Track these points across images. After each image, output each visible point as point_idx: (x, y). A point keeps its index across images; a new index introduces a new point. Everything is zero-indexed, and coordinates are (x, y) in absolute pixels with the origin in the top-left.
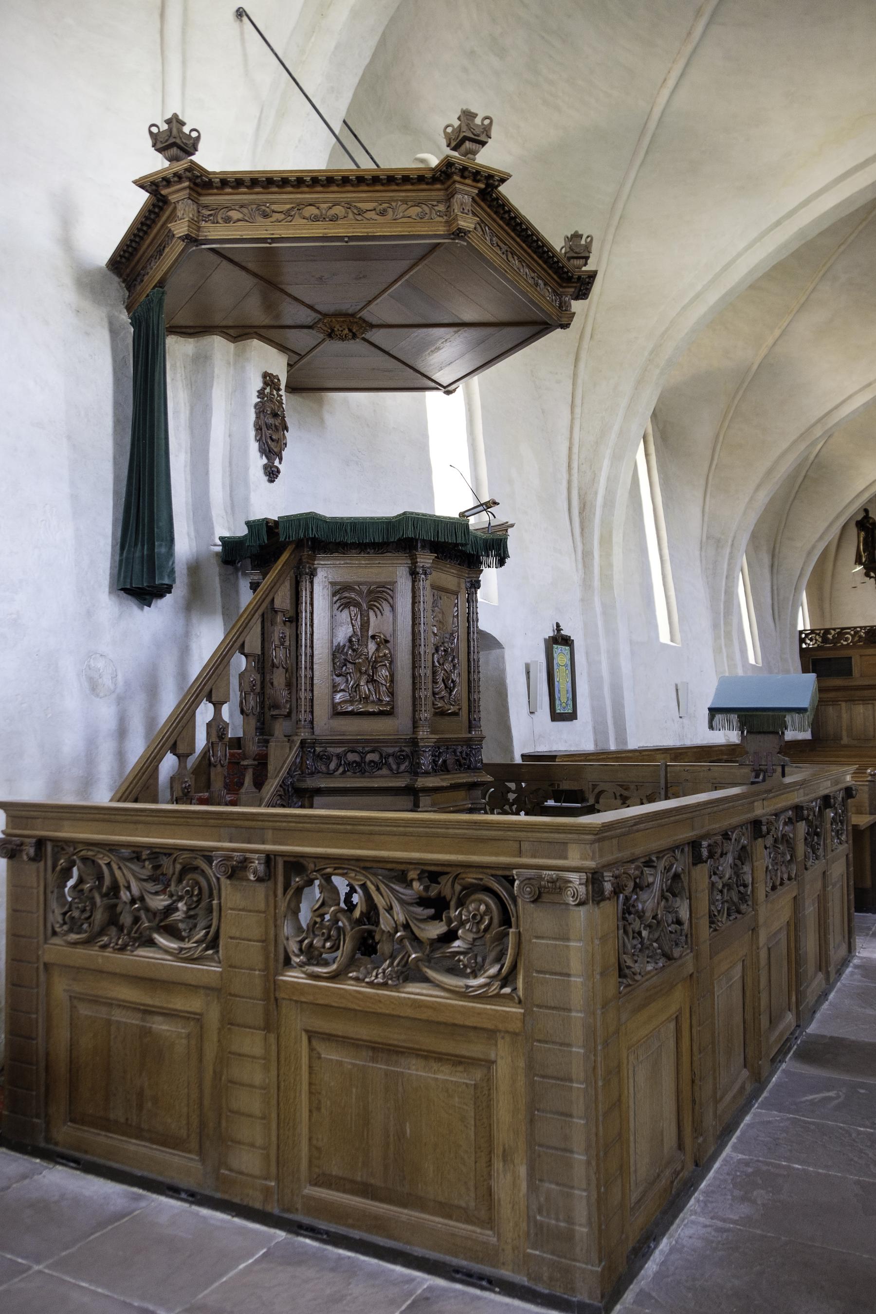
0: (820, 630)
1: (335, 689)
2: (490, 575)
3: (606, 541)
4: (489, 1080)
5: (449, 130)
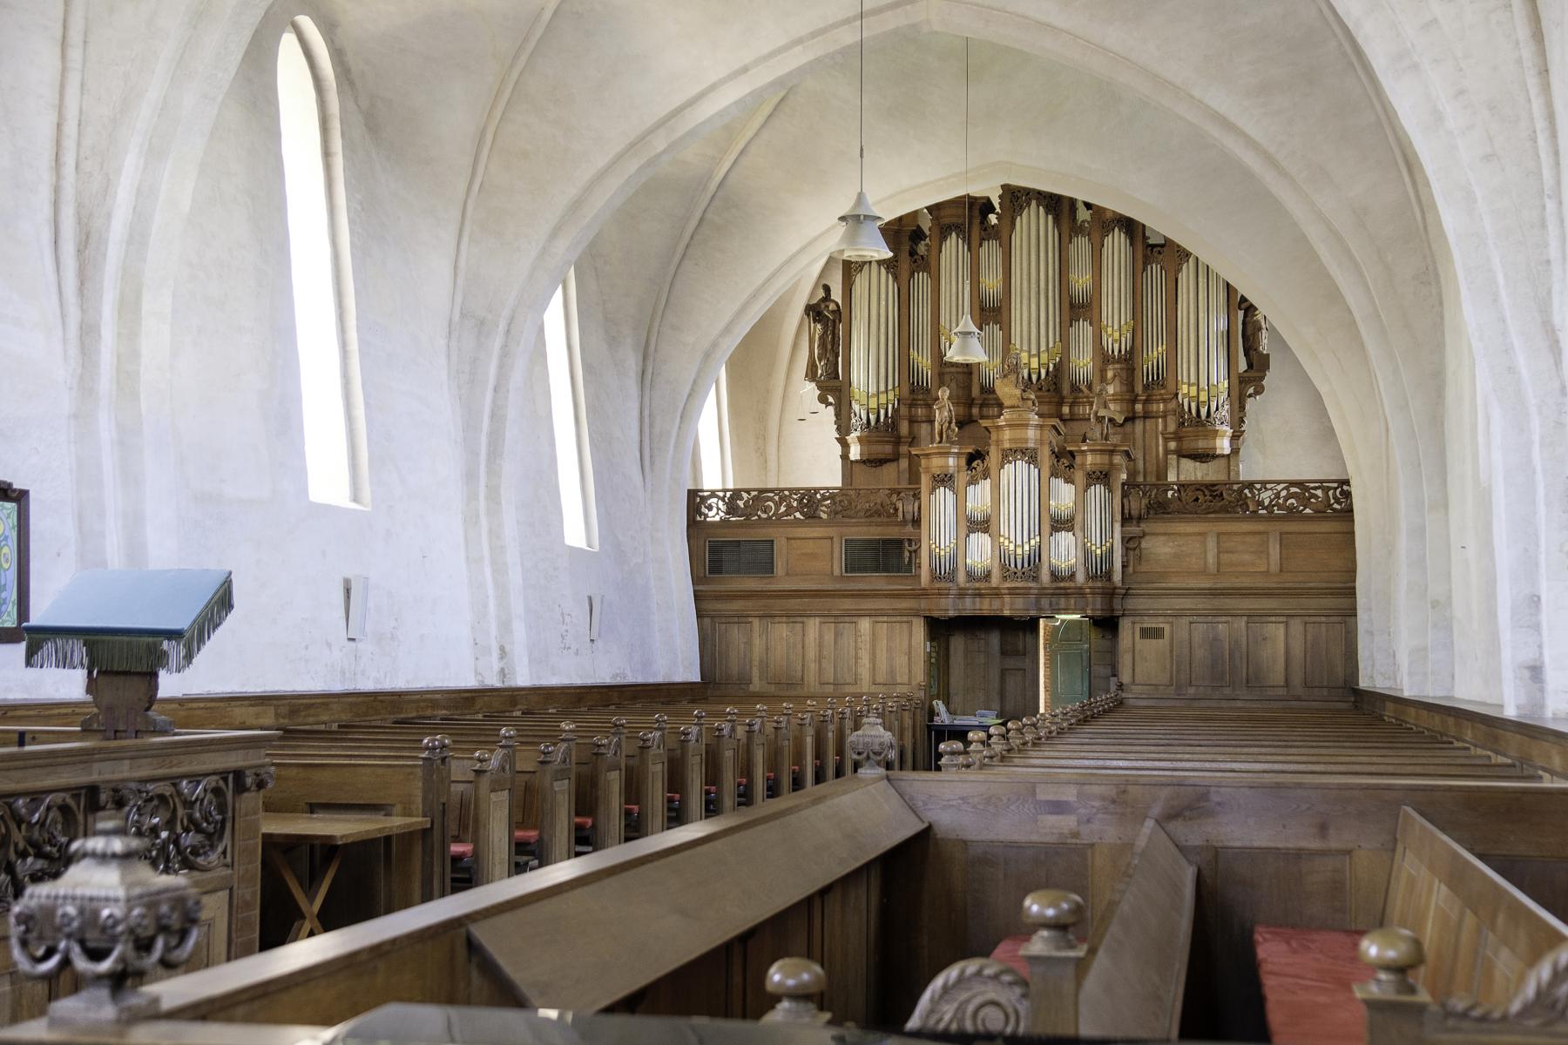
3: (130, 308)
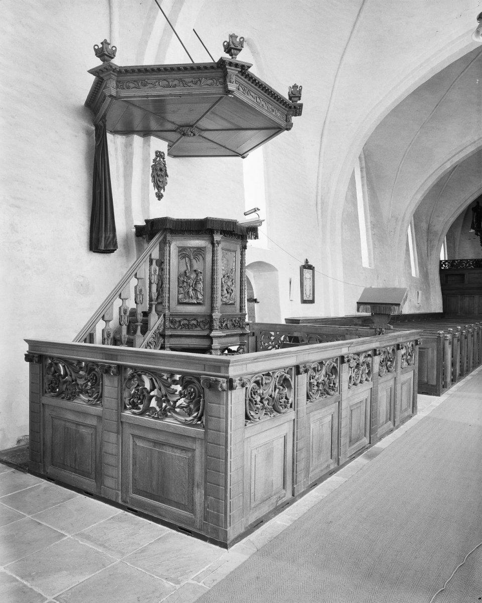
0: (450, 260)
1: (179, 294)
2: (251, 243)
4: (193, 456)
5: (225, 44)
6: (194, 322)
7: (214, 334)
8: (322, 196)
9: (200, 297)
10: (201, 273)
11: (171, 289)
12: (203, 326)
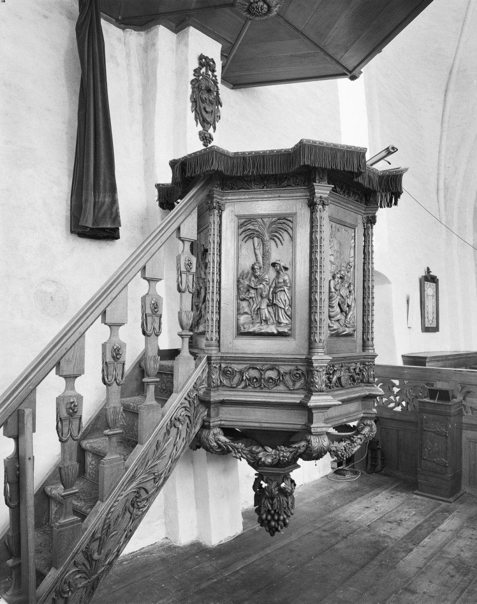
1: (239, 312)
6: (272, 374)
7: (315, 400)
8: (445, 179)
9: (284, 320)
10: (286, 269)
11: (222, 305)
12: (291, 384)
